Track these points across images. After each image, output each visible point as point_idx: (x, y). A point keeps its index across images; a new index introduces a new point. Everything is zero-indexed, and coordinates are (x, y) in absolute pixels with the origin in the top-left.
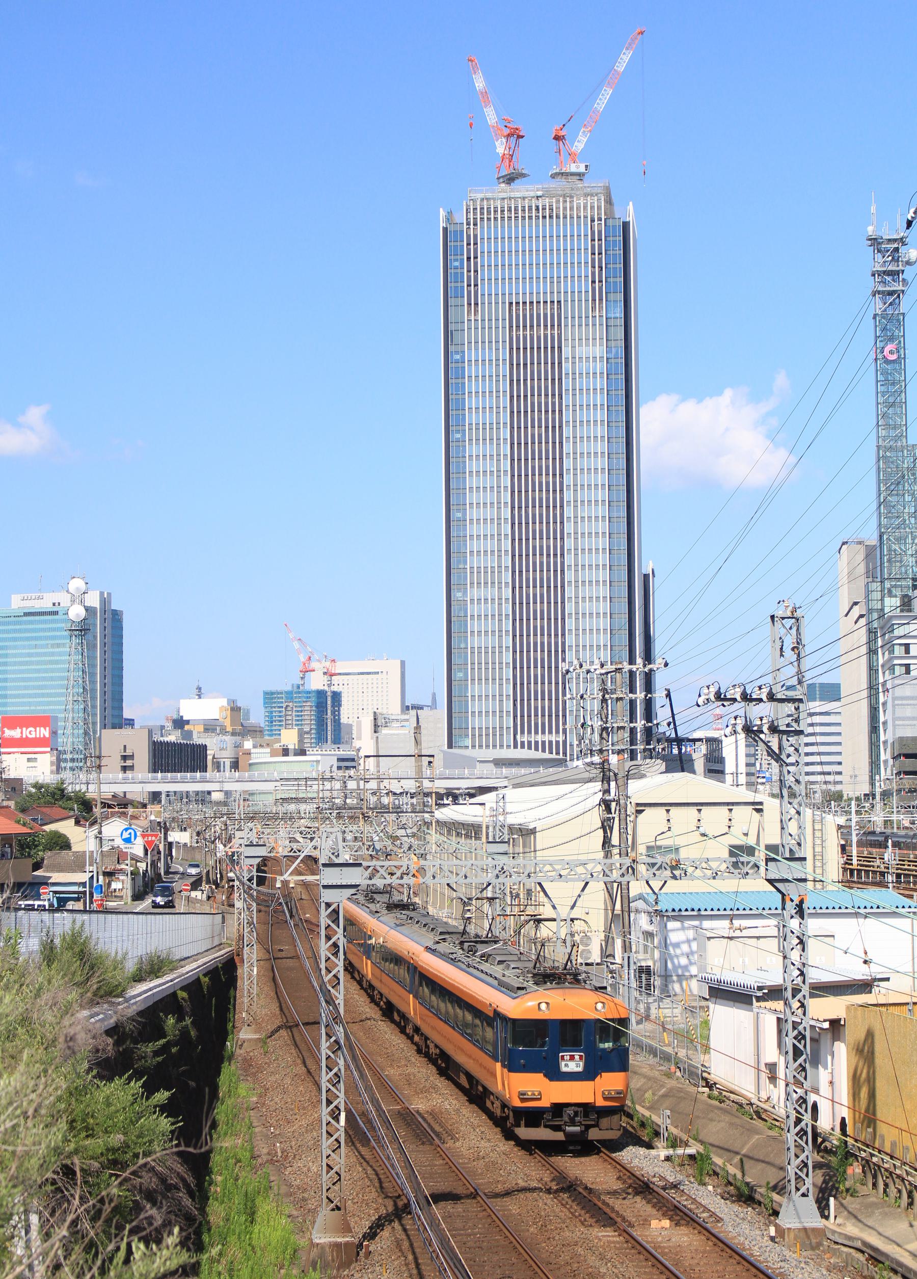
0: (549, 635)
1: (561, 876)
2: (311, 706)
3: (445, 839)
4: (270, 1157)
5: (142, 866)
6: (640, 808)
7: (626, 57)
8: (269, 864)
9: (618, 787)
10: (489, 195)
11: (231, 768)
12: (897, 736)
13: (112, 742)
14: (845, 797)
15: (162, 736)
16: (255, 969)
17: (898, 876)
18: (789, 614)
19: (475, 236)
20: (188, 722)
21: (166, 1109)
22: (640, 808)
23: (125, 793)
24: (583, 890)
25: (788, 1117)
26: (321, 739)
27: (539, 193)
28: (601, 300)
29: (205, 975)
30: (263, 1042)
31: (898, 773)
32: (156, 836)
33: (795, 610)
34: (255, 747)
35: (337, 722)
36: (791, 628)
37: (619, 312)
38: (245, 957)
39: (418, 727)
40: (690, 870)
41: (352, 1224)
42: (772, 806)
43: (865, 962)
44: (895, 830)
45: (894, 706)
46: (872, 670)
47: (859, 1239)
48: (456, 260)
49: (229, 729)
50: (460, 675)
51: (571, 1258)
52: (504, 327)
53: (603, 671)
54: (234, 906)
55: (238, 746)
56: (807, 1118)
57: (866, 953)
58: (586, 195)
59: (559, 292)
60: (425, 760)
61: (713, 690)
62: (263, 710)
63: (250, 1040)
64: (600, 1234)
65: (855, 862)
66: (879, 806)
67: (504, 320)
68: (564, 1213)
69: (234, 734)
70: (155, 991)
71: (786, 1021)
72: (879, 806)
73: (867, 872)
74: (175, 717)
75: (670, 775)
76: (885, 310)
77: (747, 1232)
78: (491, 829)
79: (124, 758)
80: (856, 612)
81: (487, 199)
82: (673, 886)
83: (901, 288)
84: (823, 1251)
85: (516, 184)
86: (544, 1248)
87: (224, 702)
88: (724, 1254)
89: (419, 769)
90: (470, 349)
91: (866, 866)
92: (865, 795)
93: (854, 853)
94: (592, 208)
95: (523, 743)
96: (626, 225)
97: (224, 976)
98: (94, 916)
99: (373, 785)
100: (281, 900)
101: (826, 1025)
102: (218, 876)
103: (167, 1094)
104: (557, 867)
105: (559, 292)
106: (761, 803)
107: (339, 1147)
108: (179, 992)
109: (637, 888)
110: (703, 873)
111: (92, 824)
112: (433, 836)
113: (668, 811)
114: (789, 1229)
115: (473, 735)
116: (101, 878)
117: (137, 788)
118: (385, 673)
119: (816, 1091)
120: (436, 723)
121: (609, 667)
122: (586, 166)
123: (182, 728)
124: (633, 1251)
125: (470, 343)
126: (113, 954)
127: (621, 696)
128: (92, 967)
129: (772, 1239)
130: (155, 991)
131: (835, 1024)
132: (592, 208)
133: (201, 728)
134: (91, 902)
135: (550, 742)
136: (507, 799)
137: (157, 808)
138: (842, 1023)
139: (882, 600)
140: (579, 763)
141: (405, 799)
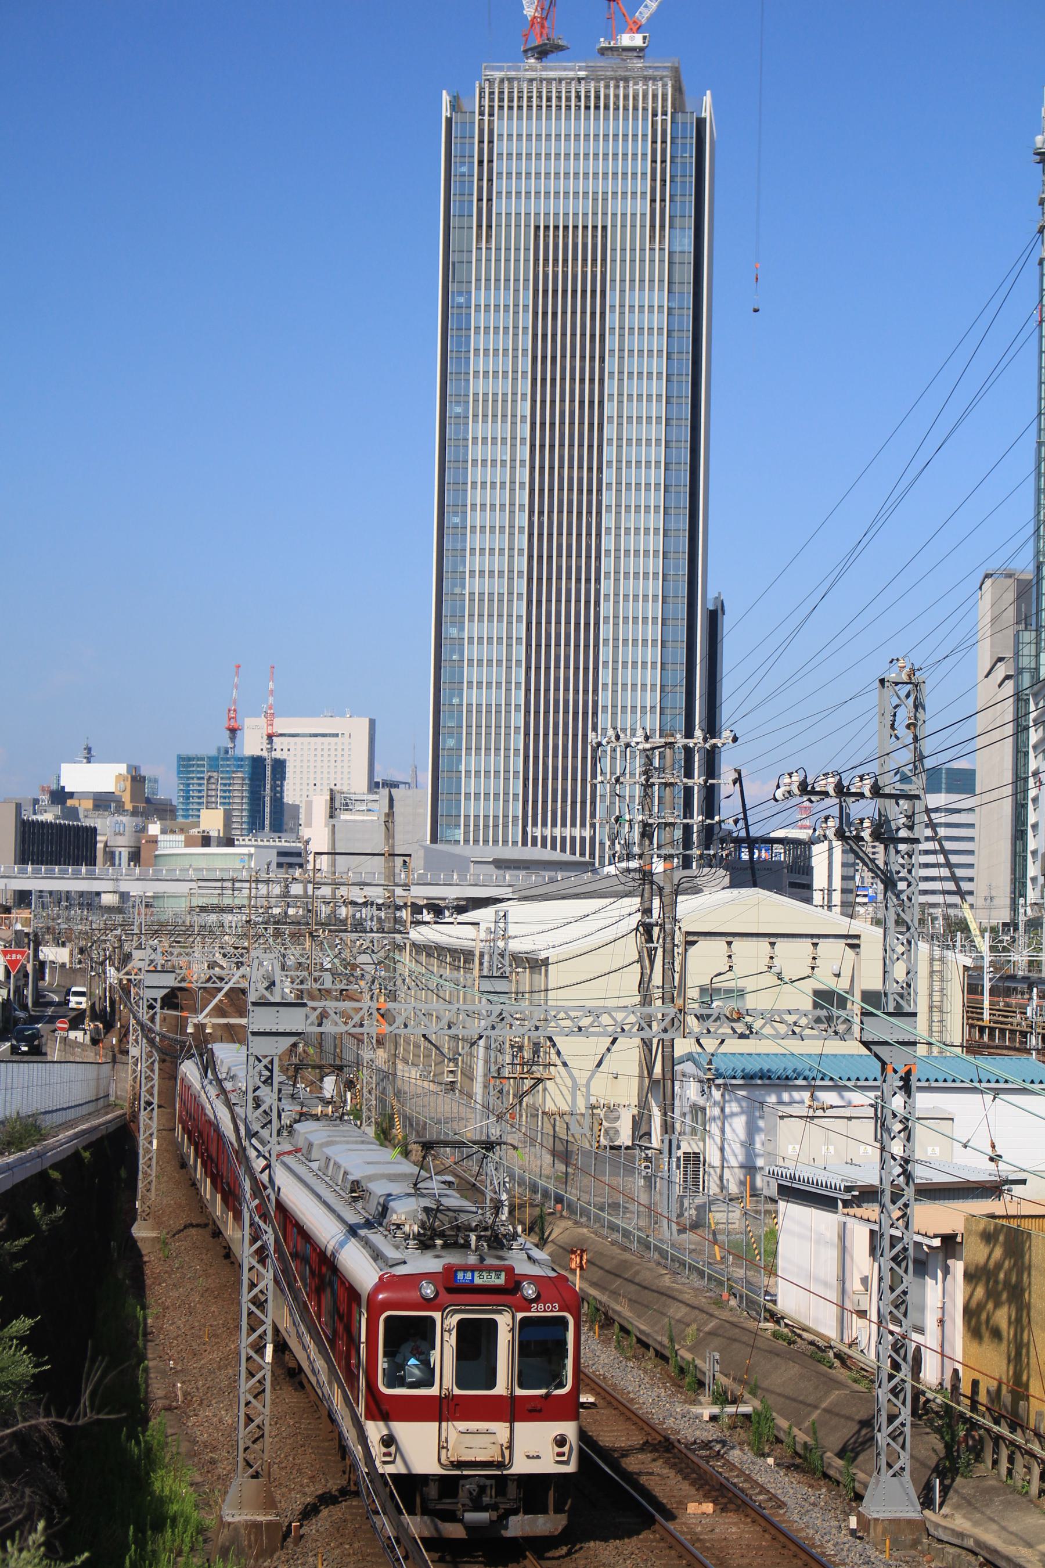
1: (580, 1029)
2: (243, 779)
3: (424, 970)
6: (691, 939)
8: (179, 994)
10: (512, 74)
11: (130, 860)
15: (35, 813)
16: (155, 1142)
18: (905, 678)
20: (71, 795)
21: (31, 1342)
22: (691, 939)
26: (255, 824)
27: (582, 74)
29: (85, 1148)
32: (22, 953)
33: (913, 671)
36: (908, 696)
37: (687, 243)
39: (390, 815)
40: (757, 1025)
41: (278, 1497)
42: (872, 936)
43: (992, 1159)
46: (1020, 754)
47: (970, 1536)
49: (129, 806)
52: (527, 260)
53: (648, 746)
54: (127, 1052)
55: (144, 829)
56: (905, 1372)
57: (993, 1146)
58: (646, 79)
59: (605, 214)
60: (399, 861)
65: (986, 1016)
66: (1022, 939)
67: (527, 249)
69: (134, 813)
71: (882, 1235)
72: (1022, 939)
73: (1002, 1031)
74: (54, 787)
75: (735, 891)
77: (818, 1522)
78: (486, 958)
80: (1001, 671)
84: (921, 1552)
85: (550, 61)
87: (122, 768)
88: (786, 1552)
89: (391, 874)
90: (478, 288)
91: (1002, 1023)
92: (1004, 924)
93: (986, 1004)
94: (655, 96)
95: (534, 838)
96: (701, 123)
99: (326, 891)
101: (937, 1242)
103: (29, 1322)
105: (605, 214)
106: (858, 937)
107: (264, 1391)
109: (683, 1047)
110: (773, 1027)
112: (406, 961)
113: (729, 943)
118: (347, 736)
119: (921, 1330)
120: (415, 807)
121: (658, 740)
122: (645, 38)
123: (63, 803)
125: (478, 280)
129: (853, 1533)
132: (655, 96)
133: (89, 804)
135: (573, 839)
136: (510, 919)
137: (25, 914)
138: (959, 1239)
140: (611, 870)
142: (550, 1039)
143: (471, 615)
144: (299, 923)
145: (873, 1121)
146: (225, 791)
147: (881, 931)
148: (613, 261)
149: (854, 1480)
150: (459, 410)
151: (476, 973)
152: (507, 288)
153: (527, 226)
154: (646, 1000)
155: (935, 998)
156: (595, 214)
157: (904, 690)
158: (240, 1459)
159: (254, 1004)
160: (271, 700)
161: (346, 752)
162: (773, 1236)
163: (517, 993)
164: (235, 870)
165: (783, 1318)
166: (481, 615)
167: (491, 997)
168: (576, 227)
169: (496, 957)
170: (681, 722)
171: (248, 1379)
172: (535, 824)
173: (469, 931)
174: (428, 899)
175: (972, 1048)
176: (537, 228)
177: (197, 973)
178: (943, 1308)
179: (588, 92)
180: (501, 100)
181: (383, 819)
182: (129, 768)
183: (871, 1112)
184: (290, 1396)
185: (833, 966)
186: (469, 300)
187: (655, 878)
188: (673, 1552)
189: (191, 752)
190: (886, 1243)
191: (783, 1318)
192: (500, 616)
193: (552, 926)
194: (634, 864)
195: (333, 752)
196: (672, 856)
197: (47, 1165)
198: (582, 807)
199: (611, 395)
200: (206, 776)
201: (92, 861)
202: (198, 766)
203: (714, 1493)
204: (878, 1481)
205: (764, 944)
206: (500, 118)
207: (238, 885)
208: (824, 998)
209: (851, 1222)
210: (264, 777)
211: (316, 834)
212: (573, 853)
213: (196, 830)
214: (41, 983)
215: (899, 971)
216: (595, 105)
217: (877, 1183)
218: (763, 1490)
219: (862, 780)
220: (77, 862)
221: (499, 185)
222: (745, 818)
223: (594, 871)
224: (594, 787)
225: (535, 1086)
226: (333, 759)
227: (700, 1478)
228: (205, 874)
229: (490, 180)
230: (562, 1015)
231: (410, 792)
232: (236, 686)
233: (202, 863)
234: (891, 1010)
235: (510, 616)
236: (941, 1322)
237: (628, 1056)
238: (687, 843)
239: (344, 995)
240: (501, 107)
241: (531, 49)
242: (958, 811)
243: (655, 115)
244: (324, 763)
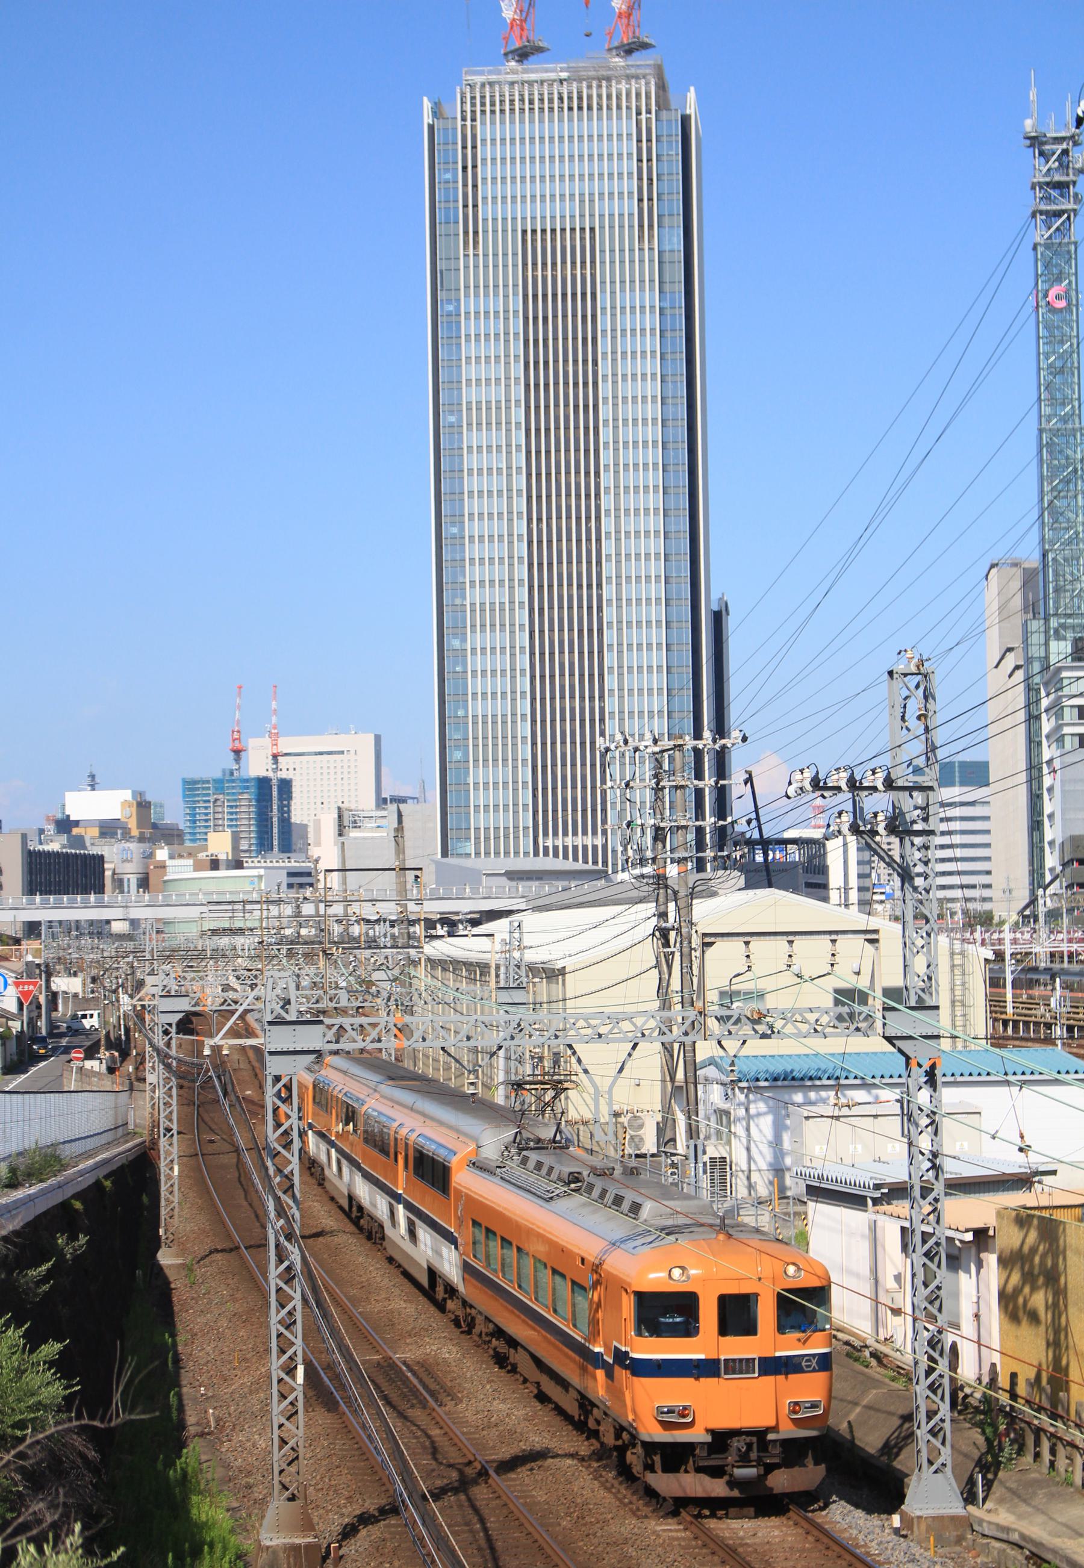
0: (582, 698)
1: (600, 1036)
2: (250, 800)
5: (16, 1026)
6: (708, 940)
9: (678, 909)
10: (493, 78)
11: (139, 886)
12: (1069, 833)
14: (996, 920)
15: (41, 843)
16: (176, 1168)
17: (1070, 1029)
18: (914, 669)
20: (77, 823)
21: (62, 1366)
25: (916, 1363)
26: (264, 845)
27: (564, 75)
28: (651, 226)
29: (106, 1177)
30: (188, 1268)
31: (1070, 886)
33: (922, 662)
34: (171, 857)
35: (285, 822)
40: (778, 1025)
41: (316, 1520)
42: (891, 932)
43: (1021, 1150)
44: (1066, 965)
45: (1063, 792)
46: (1033, 743)
49: (135, 832)
50: (458, 755)
51: (619, 1562)
52: (515, 265)
53: (657, 749)
54: (144, 1080)
56: (943, 1366)
57: (1022, 1137)
58: (629, 78)
59: (592, 215)
61: (808, 774)
62: (182, 805)
64: (659, 1528)
65: (1010, 1010)
67: (515, 254)
68: (609, 1499)
69: (141, 839)
71: (913, 1231)
73: (1026, 1024)
74: (59, 816)
75: (751, 893)
76: (1050, 237)
77: (861, 1522)
78: (502, 969)
80: (1011, 661)
83: (1071, 206)
84: (966, 1548)
85: (532, 63)
86: (581, 1548)
87: (127, 795)
88: (830, 1553)
89: (402, 890)
90: (467, 296)
93: (1009, 997)
94: (638, 95)
95: (546, 849)
96: (685, 120)
99: (337, 909)
100: (211, 1073)
101: (969, 1237)
103: (58, 1346)
104: (593, 1022)
105: (592, 215)
106: (876, 931)
109: (705, 1050)
110: (796, 1028)
112: (422, 977)
113: (747, 943)
114: (920, 1517)
115: (477, 838)
119: (957, 1326)
121: (666, 743)
123: (69, 832)
124: (704, 1551)
125: (467, 287)
129: (897, 1531)
131: (981, 1234)
132: (638, 95)
133: (95, 832)
136: (525, 929)
137: (35, 944)
138: (991, 1233)
139: (1047, 644)
140: (622, 876)
141: (379, 929)
144: (313, 943)
146: (231, 813)
147: (900, 927)
150: (452, 419)
151: (493, 984)
152: (496, 295)
153: (514, 231)
154: (666, 1005)
155: (958, 993)
156: (582, 216)
158: (276, 1482)
159: (270, 1023)
160: (274, 720)
164: (244, 892)
167: (508, 1008)
169: (512, 968)
172: (546, 834)
175: (997, 1041)
176: (524, 232)
177: (211, 1000)
178: (978, 1303)
179: (570, 93)
180: (483, 104)
182: (134, 793)
185: (853, 963)
186: (458, 308)
187: (669, 882)
188: (716, 1558)
189: (196, 776)
190: (918, 1238)
193: (571, 934)
194: (648, 870)
195: (339, 770)
196: (685, 859)
198: (593, 814)
200: (212, 799)
201: (100, 889)
204: (919, 1479)
205: (782, 943)
207: (248, 907)
208: (846, 996)
209: (881, 1220)
210: (271, 797)
211: (325, 851)
212: (586, 862)
215: (919, 965)
216: (579, 105)
219: (874, 773)
220: (86, 891)
226: (339, 776)
229: (475, 186)
231: (418, 807)
232: (239, 707)
233: (212, 887)
235: (512, 625)
236: (977, 1316)
237: (649, 1060)
238: (700, 845)
240: (483, 112)
241: (512, 52)
242: (972, 804)
243: (639, 113)
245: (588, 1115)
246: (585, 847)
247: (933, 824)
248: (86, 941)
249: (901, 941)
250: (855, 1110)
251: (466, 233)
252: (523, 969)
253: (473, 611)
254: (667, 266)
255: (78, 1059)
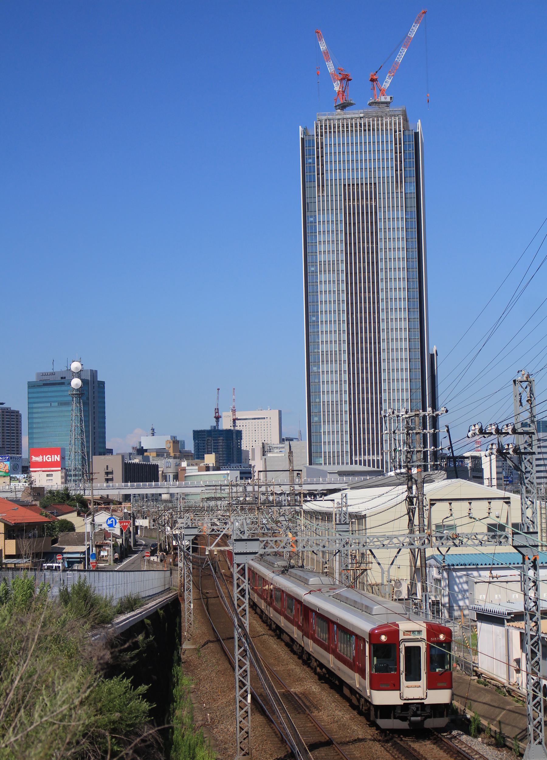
1: (384, 545)
2: (223, 440)
3: (309, 522)
4: (203, 722)
5: (119, 541)
6: (433, 502)
7: (415, 28)
10: (330, 117)
13: (99, 463)
15: (130, 460)
16: (192, 605)
18: (525, 379)
19: (322, 143)
20: (146, 451)
22: (433, 502)
23: (108, 495)
24: (398, 553)
25: (528, 695)
27: (362, 115)
28: (401, 182)
29: (161, 609)
32: (128, 522)
33: (528, 376)
34: (188, 465)
35: (240, 450)
36: (526, 388)
37: (413, 189)
38: (186, 598)
39: (291, 452)
40: (465, 540)
48: (310, 158)
49: (172, 454)
50: (316, 419)
52: (341, 200)
53: (407, 416)
54: (177, 565)
55: (179, 465)
58: (391, 116)
59: (375, 178)
60: (296, 473)
61: (477, 427)
63: (189, 649)
67: (340, 195)
69: (175, 457)
70: (130, 619)
71: (526, 634)
75: (450, 481)
78: (338, 515)
79: (107, 473)
81: (329, 119)
82: (454, 550)
87: (169, 438)
89: (292, 480)
90: (319, 214)
94: (395, 124)
95: (356, 461)
96: (416, 134)
97: (173, 608)
98: (92, 573)
99: (263, 489)
102: (167, 547)
103: (146, 687)
105: (375, 178)
107: (247, 716)
108: (145, 620)
109: (429, 552)
111: (88, 515)
112: (302, 520)
113: (450, 504)
115: (325, 457)
116: (94, 548)
117: (116, 492)
118: (269, 418)
120: (301, 448)
121: (410, 414)
122: (391, 98)
123: (143, 454)
125: (319, 210)
126: (104, 597)
127: (419, 431)
128: (92, 606)
130: (130, 619)
132: (395, 124)
133: (154, 454)
134: (89, 564)
136: (348, 498)
137: (128, 505)
140: (392, 474)
141: (282, 498)
142: (371, 551)
143: (323, 361)
144: (252, 504)
145: (520, 583)
147: (520, 496)
148: (380, 198)
149: (519, 747)
150: (313, 269)
151: (334, 522)
152: (332, 213)
153: (340, 185)
154: (412, 532)
156: (370, 178)
157: (524, 384)
158: (238, 747)
161: (269, 426)
162: (475, 637)
163: (352, 531)
165: (482, 674)
166: (331, 361)
168: (362, 184)
169: (342, 515)
170: (420, 405)
171: (240, 711)
173: (330, 504)
174: (309, 490)
176: (345, 185)
177: (206, 529)
180: (326, 129)
181: (288, 455)
183: (518, 578)
184: (259, 718)
185: (499, 512)
187: (413, 476)
190: (529, 638)
191: (482, 674)
192: (336, 361)
193: (367, 500)
194: (403, 470)
195: (263, 426)
196: (420, 466)
197: (144, 617)
198: (377, 445)
199: (381, 259)
202: (202, 435)
203: (455, 755)
204: (530, 747)
206: (326, 137)
207: (222, 488)
208: (491, 528)
211: (257, 464)
212: (374, 467)
213: (203, 464)
214: (136, 536)
215: (529, 513)
216: (368, 129)
217: (523, 610)
218: (477, 753)
221: (327, 167)
222: (452, 447)
223: (383, 475)
224: (382, 436)
225: (362, 573)
227: (448, 748)
228: (208, 483)
229: (322, 165)
230: (375, 540)
231: (298, 443)
233: (207, 478)
234: (526, 531)
235: (340, 361)
237: (405, 557)
238: (425, 459)
239: (274, 534)
240: (326, 132)
241: (338, 105)
243: (395, 132)
244: (257, 433)
245: (379, 581)
246: (373, 460)
247: (535, 449)
248: (150, 503)
249: (520, 502)
250: (500, 579)
251: (319, 186)
252: (348, 515)
253: (323, 355)
254: (409, 200)
255: (147, 556)
